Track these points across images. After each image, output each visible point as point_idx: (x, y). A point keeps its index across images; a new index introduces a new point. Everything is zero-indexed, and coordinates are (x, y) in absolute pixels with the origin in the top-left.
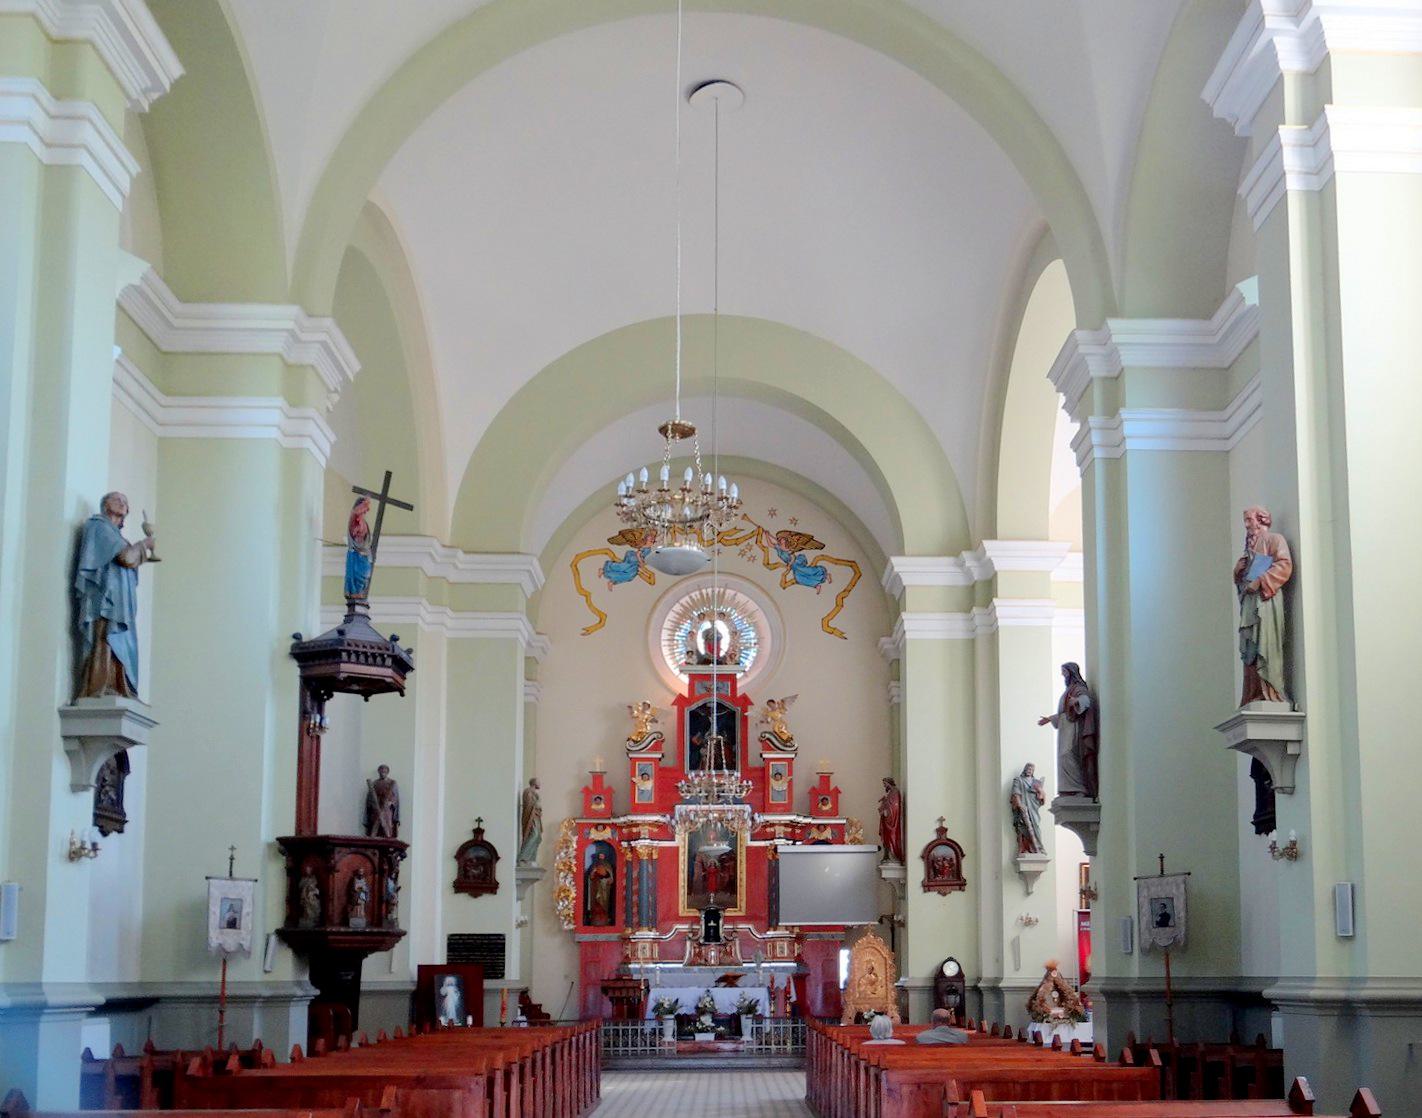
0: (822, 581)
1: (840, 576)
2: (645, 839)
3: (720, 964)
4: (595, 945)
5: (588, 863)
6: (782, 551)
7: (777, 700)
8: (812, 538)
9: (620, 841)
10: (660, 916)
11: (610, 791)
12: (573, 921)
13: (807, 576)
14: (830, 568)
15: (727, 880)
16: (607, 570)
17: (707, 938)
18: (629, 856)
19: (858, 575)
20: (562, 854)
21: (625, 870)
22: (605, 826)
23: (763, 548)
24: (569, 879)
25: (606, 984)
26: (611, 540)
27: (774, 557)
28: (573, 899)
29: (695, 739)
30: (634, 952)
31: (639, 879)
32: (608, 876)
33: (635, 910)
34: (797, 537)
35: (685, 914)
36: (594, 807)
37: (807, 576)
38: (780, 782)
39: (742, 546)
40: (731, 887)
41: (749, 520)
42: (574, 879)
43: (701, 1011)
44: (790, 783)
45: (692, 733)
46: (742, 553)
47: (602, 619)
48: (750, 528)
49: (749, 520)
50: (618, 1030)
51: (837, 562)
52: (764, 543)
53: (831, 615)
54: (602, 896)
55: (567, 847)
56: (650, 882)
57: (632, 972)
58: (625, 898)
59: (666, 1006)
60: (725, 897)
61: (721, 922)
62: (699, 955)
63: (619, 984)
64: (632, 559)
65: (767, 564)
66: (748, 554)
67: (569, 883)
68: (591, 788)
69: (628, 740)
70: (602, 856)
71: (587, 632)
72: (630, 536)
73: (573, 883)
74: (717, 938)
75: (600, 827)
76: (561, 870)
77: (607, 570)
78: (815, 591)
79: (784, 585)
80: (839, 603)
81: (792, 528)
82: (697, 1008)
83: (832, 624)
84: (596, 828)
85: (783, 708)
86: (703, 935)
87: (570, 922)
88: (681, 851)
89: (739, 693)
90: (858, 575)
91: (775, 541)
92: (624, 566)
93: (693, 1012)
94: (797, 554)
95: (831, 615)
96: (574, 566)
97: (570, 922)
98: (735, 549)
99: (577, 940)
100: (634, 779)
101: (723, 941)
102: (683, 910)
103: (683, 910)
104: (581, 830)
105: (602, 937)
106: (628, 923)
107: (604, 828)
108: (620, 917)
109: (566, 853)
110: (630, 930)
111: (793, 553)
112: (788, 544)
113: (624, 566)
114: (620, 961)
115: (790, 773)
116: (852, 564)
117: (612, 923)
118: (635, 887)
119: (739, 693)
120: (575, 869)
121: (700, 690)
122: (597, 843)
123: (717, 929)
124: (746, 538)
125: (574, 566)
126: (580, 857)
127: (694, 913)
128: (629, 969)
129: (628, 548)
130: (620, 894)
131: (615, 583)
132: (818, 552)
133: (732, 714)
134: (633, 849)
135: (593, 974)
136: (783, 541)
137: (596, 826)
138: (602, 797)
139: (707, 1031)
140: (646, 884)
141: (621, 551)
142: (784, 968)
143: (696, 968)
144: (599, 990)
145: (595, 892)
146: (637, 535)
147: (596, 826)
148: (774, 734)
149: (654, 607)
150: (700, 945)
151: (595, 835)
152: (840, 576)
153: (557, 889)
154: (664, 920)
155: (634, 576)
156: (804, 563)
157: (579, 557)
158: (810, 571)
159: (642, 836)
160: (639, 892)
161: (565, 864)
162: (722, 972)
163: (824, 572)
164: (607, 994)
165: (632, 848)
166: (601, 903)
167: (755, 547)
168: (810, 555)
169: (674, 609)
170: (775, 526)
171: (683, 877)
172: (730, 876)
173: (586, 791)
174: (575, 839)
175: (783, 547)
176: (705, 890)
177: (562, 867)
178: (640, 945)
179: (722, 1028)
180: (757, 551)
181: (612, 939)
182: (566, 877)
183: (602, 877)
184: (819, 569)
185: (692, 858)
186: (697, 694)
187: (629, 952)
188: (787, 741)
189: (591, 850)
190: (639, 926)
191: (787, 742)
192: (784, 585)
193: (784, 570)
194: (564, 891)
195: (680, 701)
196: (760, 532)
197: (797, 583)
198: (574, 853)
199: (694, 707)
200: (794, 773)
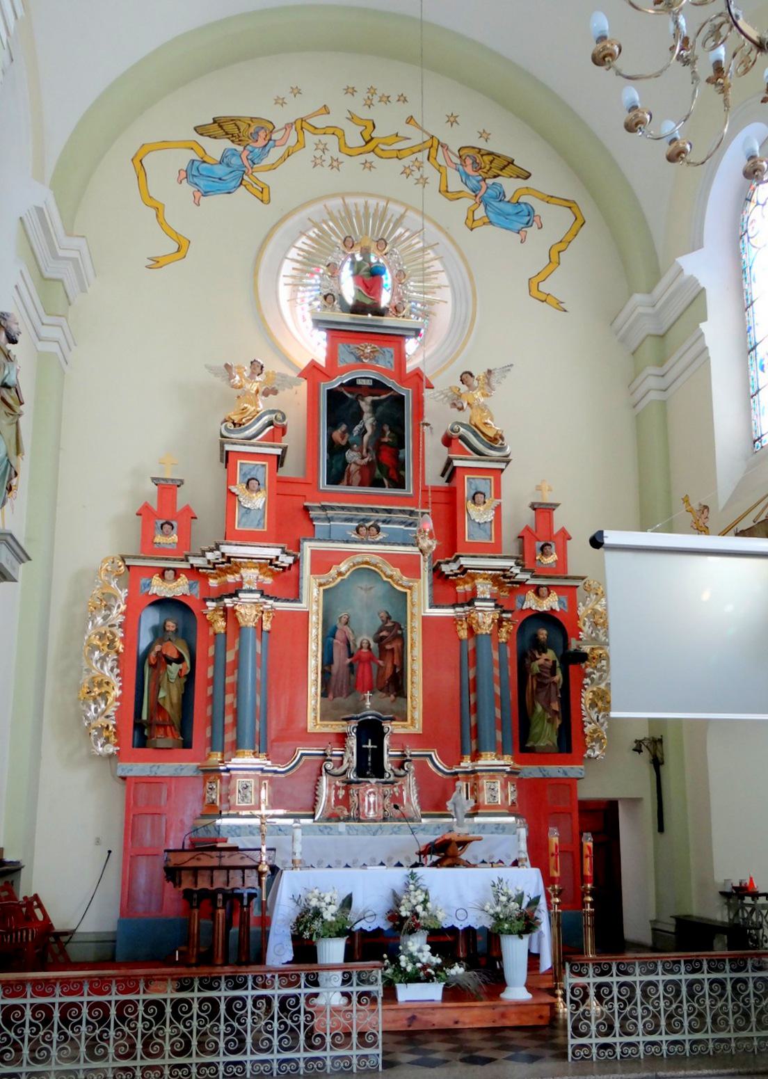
0: (528, 224)
1: (555, 221)
2: (251, 591)
3: (385, 819)
4: (153, 782)
5: (145, 640)
6: (468, 176)
7: (478, 372)
8: (511, 162)
9: (205, 600)
10: (273, 733)
11: (189, 515)
12: (112, 739)
13: (506, 215)
14: (539, 207)
15: (389, 672)
16: (192, 173)
17: (361, 771)
18: (220, 625)
19: (580, 222)
20: (99, 620)
21: (211, 652)
22: (177, 573)
23: (439, 168)
24: (109, 664)
25: (176, 860)
26: (201, 130)
27: (455, 183)
28: (117, 699)
29: (337, 435)
30: (226, 798)
31: (237, 664)
32: (180, 660)
33: (229, 719)
34: (491, 158)
35: (318, 729)
36: (159, 539)
37: (506, 215)
38: (482, 508)
39: (407, 161)
40: (396, 684)
41: (417, 125)
42: (120, 662)
43: (400, 924)
44: (498, 509)
45: (332, 424)
46: (407, 172)
47: (182, 249)
48: (417, 138)
49: (417, 125)
50: (214, 1002)
51: (550, 199)
52: (441, 160)
53: (542, 276)
54: (169, 695)
55: (109, 608)
56: (259, 671)
57: (224, 834)
58: (211, 721)
59: (328, 916)
60: (387, 700)
61: (386, 742)
62: (345, 801)
63: (207, 860)
64: (235, 161)
65: (445, 191)
66: (417, 174)
67: (108, 671)
68: (154, 506)
69: (226, 421)
70: (171, 626)
71: (156, 263)
72: (230, 128)
73: (117, 671)
74: (379, 771)
75: (169, 574)
76: (98, 648)
77: (192, 173)
78: (518, 237)
79: (471, 224)
80: (554, 258)
81: (481, 144)
82: (394, 916)
83: (542, 287)
84: (162, 576)
85: (489, 384)
86: (354, 764)
87: (107, 740)
88: (313, 619)
89: (410, 367)
90: (580, 222)
91: (458, 161)
92: (220, 171)
93: (385, 926)
94: (490, 181)
95: (542, 276)
96: (139, 163)
97: (107, 740)
98: (398, 165)
99: (120, 773)
100: (234, 489)
101: (390, 776)
102: (313, 722)
103: (313, 722)
104: (133, 574)
105: (166, 769)
106: (212, 744)
107: (177, 576)
108: (200, 732)
109: (105, 618)
110: (216, 757)
111: (484, 180)
112: (477, 167)
113: (220, 171)
114: (199, 812)
115: (498, 495)
116: (570, 205)
117: (187, 744)
118: (229, 680)
119: (410, 367)
120: (120, 646)
121: (345, 356)
122: (161, 603)
123: (378, 754)
124: (413, 151)
125: (139, 163)
126: (130, 625)
127: (337, 727)
128: (218, 829)
129: (226, 144)
130: (201, 692)
131: (205, 194)
132: (520, 183)
133: (400, 400)
134: (229, 614)
135: (148, 836)
136: (469, 161)
137: (162, 573)
138: (175, 524)
139: (428, 979)
140: (251, 673)
141: (216, 148)
142: (498, 825)
143: (342, 826)
144: (160, 873)
145: (157, 687)
146: (243, 126)
147: (162, 573)
148: (476, 430)
149: (268, 237)
150: (350, 783)
151: (160, 588)
152: (555, 221)
153: (86, 678)
154: (279, 739)
155: (236, 187)
156: (501, 197)
157: (146, 149)
158: (509, 208)
159: (246, 587)
160: (237, 689)
161: (102, 636)
162: (431, 830)
163: (530, 213)
164: (177, 884)
165: (225, 609)
166: (168, 707)
167: (427, 164)
168: (509, 185)
169: (290, 256)
170: (456, 139)
171: (314, 663)
172: (394, 667)
173: (145, 512)
174: (123, 594)
175: (469, 170)
176: (353, 687)
177: (97, 642)
178: (238, 783)
179: (457, 970)
180: (429, 170)
181: (185, 773)
182: (103, 659)
183: (170, 661)
184: (523, 206)
185: (329, 634)
186: (341, 365)
187: (215, 796)
188: (494, 440)
189: (151, 618)
190: (236, 747)
191: (495, 441)
192: (471, 224)
193: (468, 202)
194: (100, 685)
195: (313, 369)
196: (434, 145)
197: (490, 222)
198: (121, 619)
199: (335, 384)
200: (503, 494)
